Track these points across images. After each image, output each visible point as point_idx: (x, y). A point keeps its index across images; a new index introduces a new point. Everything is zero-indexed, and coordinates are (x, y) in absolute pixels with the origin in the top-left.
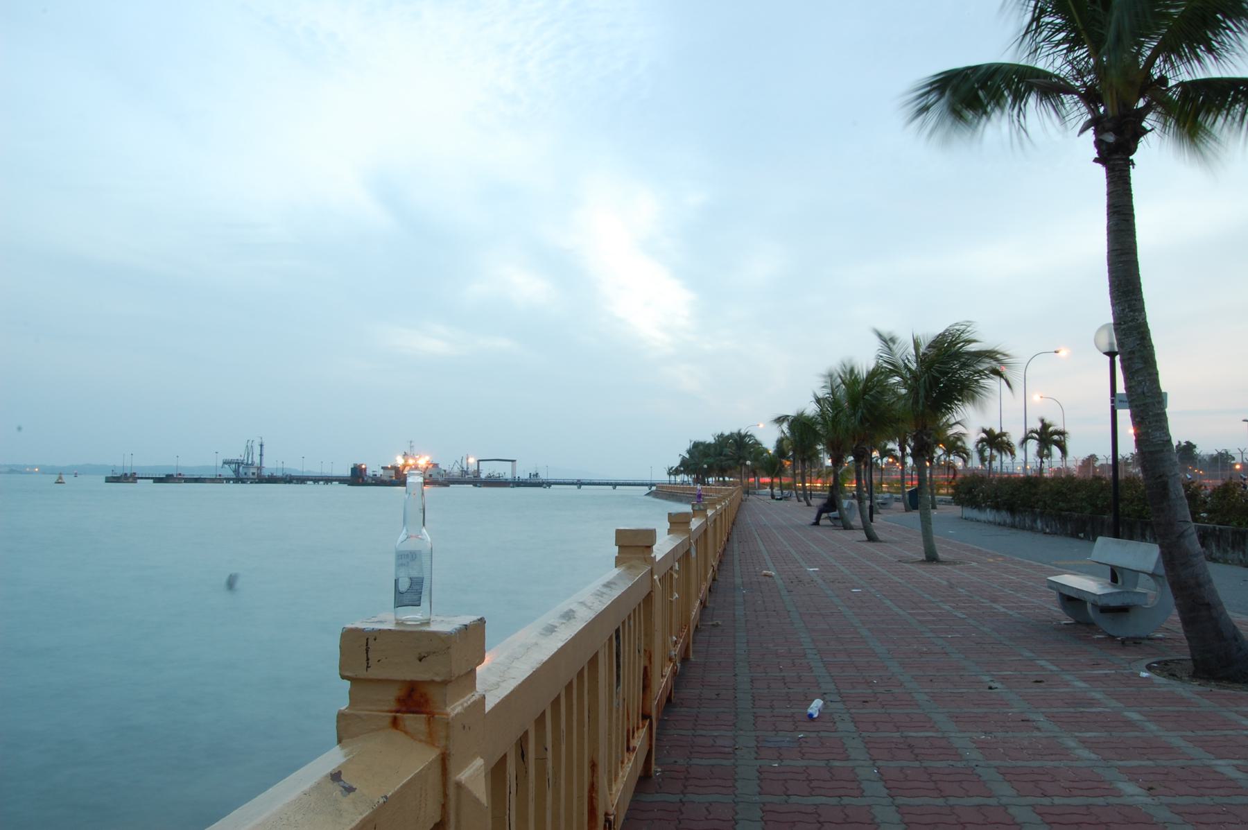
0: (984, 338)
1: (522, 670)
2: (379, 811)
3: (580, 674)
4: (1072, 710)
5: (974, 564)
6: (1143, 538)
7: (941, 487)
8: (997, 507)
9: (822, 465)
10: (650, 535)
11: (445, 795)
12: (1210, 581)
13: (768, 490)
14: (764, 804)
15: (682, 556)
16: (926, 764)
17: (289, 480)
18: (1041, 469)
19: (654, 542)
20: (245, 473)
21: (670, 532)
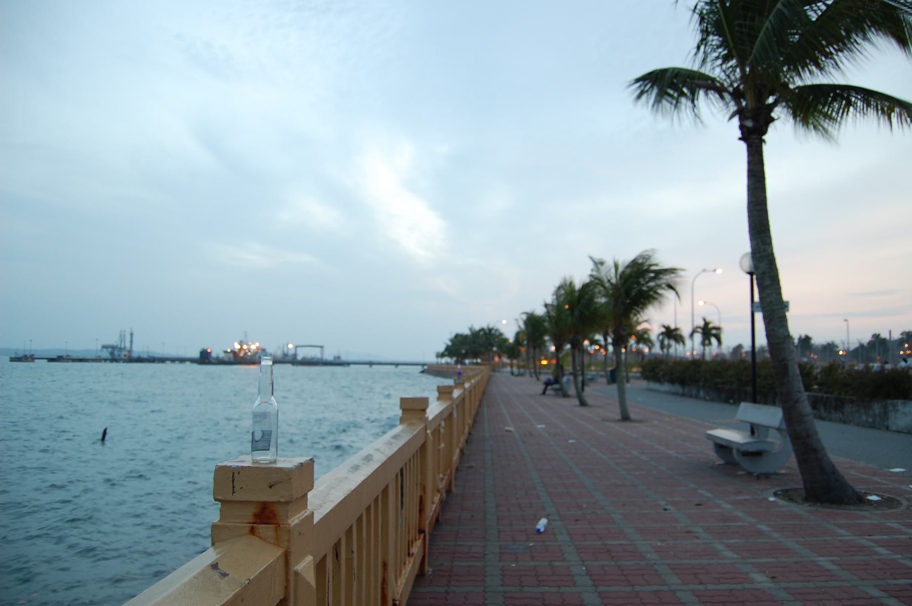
0: (663, 261)
1: (338, 496)
2: (245, 589)
3: (376, 500)
4: (721, 524)
5: (656, 422)
6: (774, 403)
7: (632, 366)
8: (672, 382)
9: (548, 351)
10: (424, 402)
11: (287, 580)
12: (816, 433)
13: (509, 369)
14: (505, 592)
15: (447, 416)
16: (619, 563)
17: (152, 360)
18: (703, 355)
19: (427, 407)
20: (118, 355)
21: (438, 399)
